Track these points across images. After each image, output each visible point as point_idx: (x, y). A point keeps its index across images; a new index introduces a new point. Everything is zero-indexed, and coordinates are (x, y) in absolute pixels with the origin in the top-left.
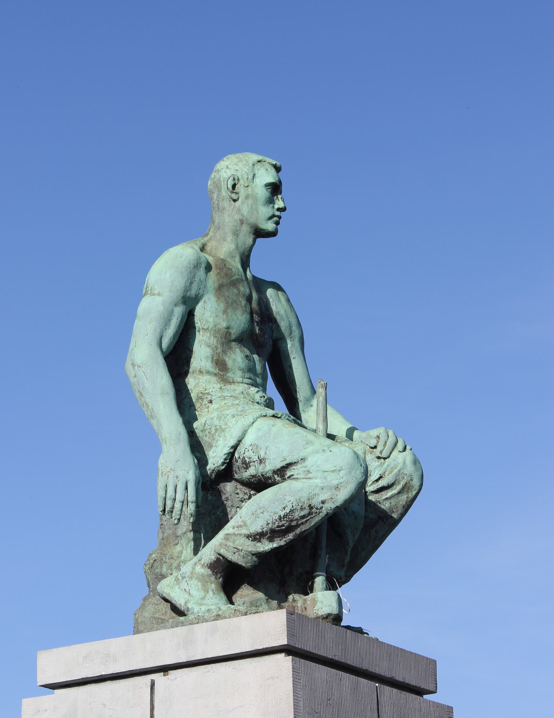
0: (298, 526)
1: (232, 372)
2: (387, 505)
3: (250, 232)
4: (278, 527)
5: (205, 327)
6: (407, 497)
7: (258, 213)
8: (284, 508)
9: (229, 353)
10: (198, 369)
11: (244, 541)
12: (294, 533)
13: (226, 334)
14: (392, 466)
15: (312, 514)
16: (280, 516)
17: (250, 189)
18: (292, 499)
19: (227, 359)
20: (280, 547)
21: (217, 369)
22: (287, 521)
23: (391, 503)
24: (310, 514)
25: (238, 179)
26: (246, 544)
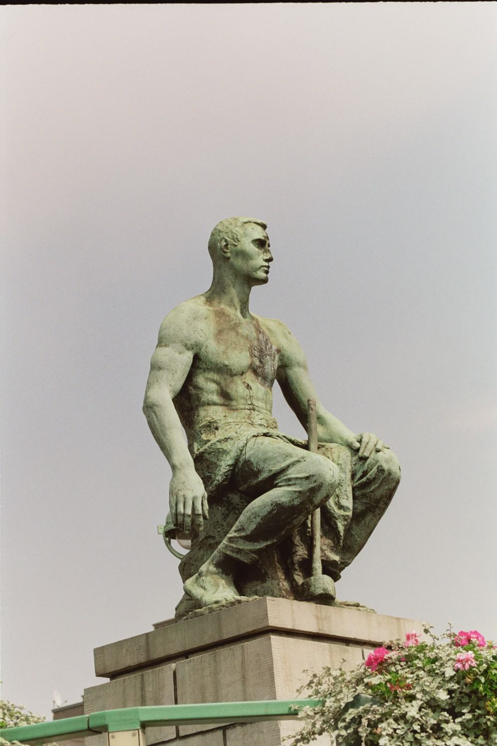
1: (235, 401)
3: (244, 283)
19: (229, 391)
21: (223, 401)
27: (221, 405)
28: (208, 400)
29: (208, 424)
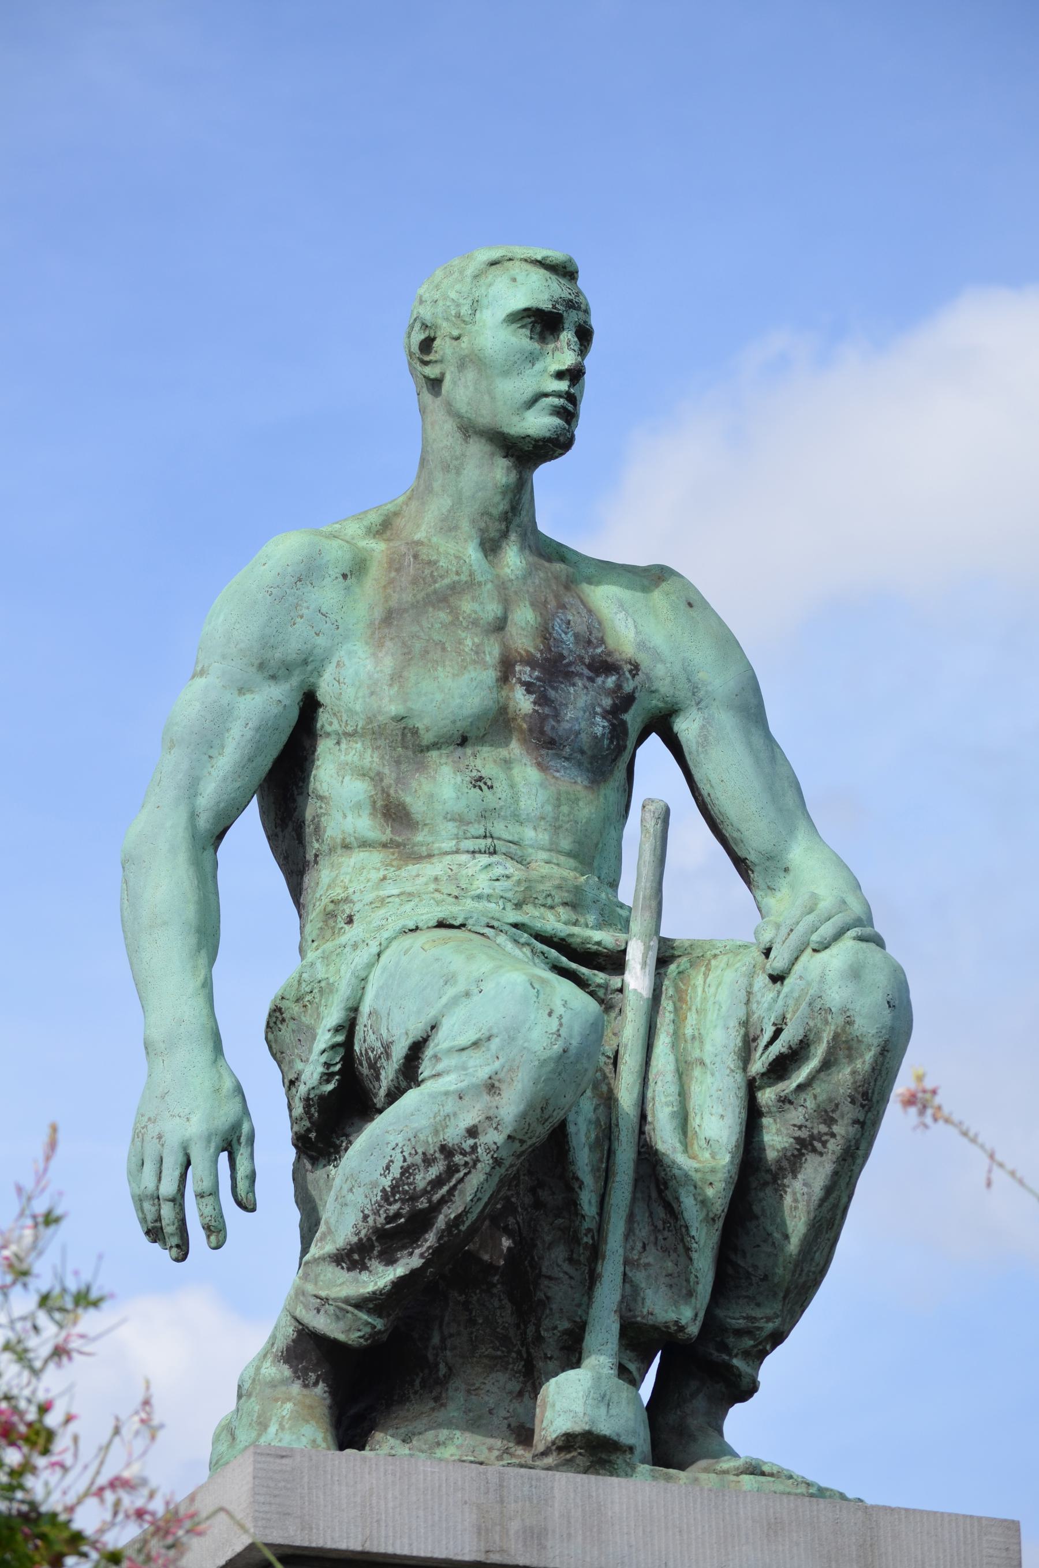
0: (435, 1208)
1: (426, 829)
2: (808, 1104)
3: (493, 454)
4: (389, 1219)
5: (349, 729)
6: (854, 1073)
7: (493, 398)
8: (388, 1168)
9: (414, 784)
10: (339, 841)
11: (333, 1273)
12: (434, 1230)
13: (404, 735)
14: (796, 995)
15: (458, 1171)
16: (384, 1190)
17: (465, 343)
18: (400, 1139)
19: (408, 800)
20: (414, 1273)
21: (389, 830)
22: (403, 1201)
23: (815, 1097)
24: (452, 1170)
25: (435, 327)
26: (339, 1282)
27: (385, 846)
28: (343, 832)
29: (331, 907)
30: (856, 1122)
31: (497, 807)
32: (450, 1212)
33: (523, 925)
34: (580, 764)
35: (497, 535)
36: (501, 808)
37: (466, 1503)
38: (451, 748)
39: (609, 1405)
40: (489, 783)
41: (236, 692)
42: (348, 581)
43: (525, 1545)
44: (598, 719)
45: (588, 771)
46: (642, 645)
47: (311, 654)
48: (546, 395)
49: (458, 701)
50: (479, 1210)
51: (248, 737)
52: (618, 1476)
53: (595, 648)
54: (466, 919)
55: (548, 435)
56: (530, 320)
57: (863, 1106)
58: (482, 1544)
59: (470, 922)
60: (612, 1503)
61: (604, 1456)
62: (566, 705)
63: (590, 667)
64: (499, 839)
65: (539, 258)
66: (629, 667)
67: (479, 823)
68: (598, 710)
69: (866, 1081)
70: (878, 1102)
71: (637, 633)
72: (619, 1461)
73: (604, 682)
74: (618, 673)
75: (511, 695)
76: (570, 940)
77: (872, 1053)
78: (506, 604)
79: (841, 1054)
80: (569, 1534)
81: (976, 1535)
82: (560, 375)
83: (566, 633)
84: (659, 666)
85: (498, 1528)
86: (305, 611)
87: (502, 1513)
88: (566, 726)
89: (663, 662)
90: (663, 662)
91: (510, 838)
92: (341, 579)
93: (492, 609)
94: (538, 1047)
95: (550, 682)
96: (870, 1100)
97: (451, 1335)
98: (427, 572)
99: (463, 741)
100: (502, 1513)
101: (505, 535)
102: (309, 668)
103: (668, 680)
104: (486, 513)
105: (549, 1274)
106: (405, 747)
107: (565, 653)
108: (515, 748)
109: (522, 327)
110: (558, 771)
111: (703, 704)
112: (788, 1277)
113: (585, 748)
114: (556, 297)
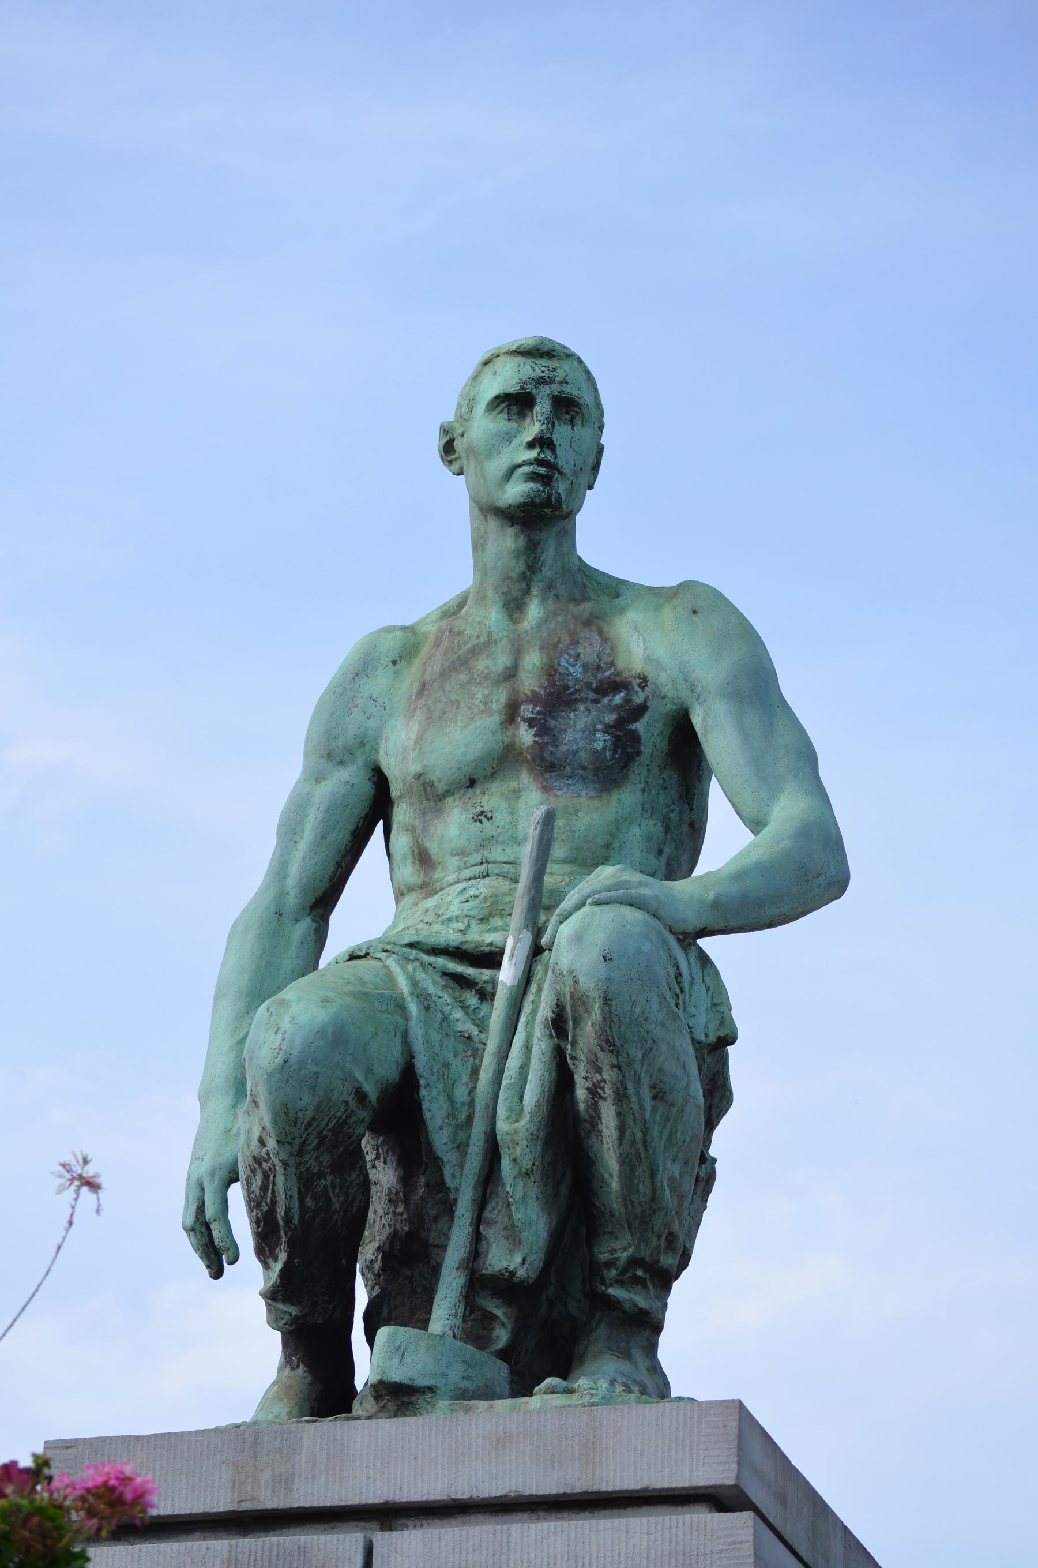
3: (502, 526)
13: (425, 789)
30: (613, 1066)
31: (495, 834)
32: (281, 1211)
33: (418, 943)
34: (584, 778)
35: (519, 594)
36: (499, 835)
37: (223, 1462)
38: (462, 791)
39: (403, 1354)
40: (489, 816)
41: (314, 782)
42: (398, 666)
43: (274, 1491)
44: (598, 735)
45: (595, 782)
46: (648, 660)
47: (365, 736)
48: (519, 466)
49: (462, 750)
50: (297, 1205)
51: (320, 819)
52: (421, 1414)
53: (606, 671)
54: (368, 948)
55: (522, 500)
56: (504, 405)
57: (611, 1052)
58: (236, 1495)
59: (371, 950)
60: (355, 1442)
61: (406, 1399)
62: (565, 731)
63: (596, 691)
64: (494, 862)
65: (514, 348)
66: (638, 681)
67: (478, 852)
68: (599, 727)
69: (603, 1030)
70: (622, 1046)
71: (645, 649)
72: (419, 1402)
73: (610, 701)
74: (627, 689)
75: (516, 733)
76: (465, 947)
77: (597, 1006)
78: (517, 653)
79: (581, 1009)
80: (314, 1476)
81: (696, 1418)
82: (531, 445)
83: (573, 666)
84: (662, 674)
85: (250, 1480)
86: (360, 701)
87: (255, 1466)
88: (563, 748)
89: (664, 670)
90: (664, 670)
91: (506, 859)
92: (391, 666)
93: (502, 660)
94: (265, 1063)
95: (550, 712)
96: (614, 1046)
97: (396, 1307)
98: (456, 642)
99: (472, 783)
100: (255, 1466)
101: (527, 592)
102: (368, 748)
103: (670, 684)
104: (507, 578)
105: (436, 1243)
106: (428, 799)
107: (571, 683)
108: (525, 778)
109: (501, 412)
110: (561, 790)
111: (701, 699)
112: (623, 1210)
113: (585, 764)
114: (525, 378)
